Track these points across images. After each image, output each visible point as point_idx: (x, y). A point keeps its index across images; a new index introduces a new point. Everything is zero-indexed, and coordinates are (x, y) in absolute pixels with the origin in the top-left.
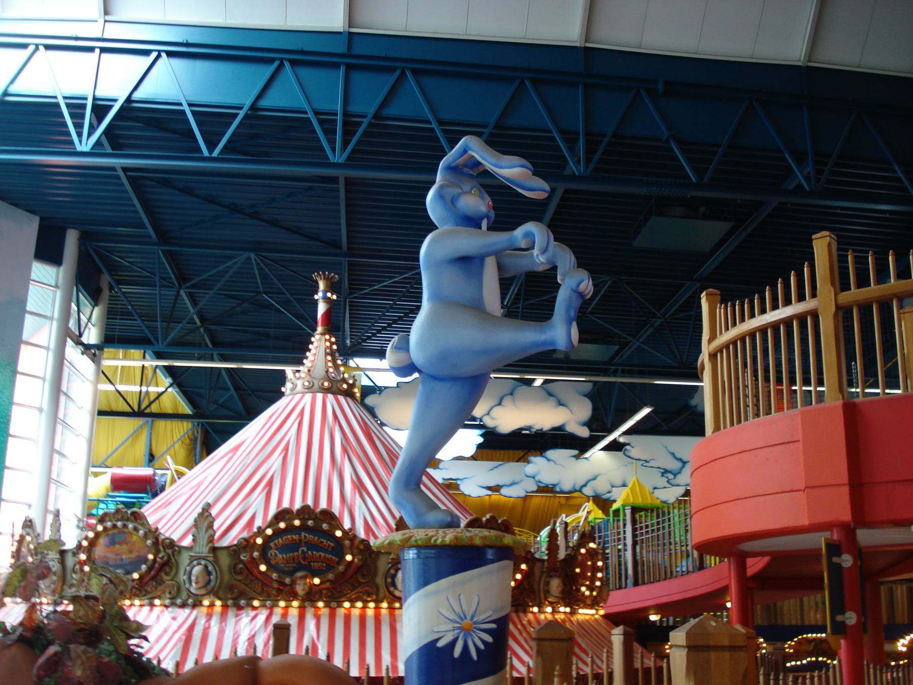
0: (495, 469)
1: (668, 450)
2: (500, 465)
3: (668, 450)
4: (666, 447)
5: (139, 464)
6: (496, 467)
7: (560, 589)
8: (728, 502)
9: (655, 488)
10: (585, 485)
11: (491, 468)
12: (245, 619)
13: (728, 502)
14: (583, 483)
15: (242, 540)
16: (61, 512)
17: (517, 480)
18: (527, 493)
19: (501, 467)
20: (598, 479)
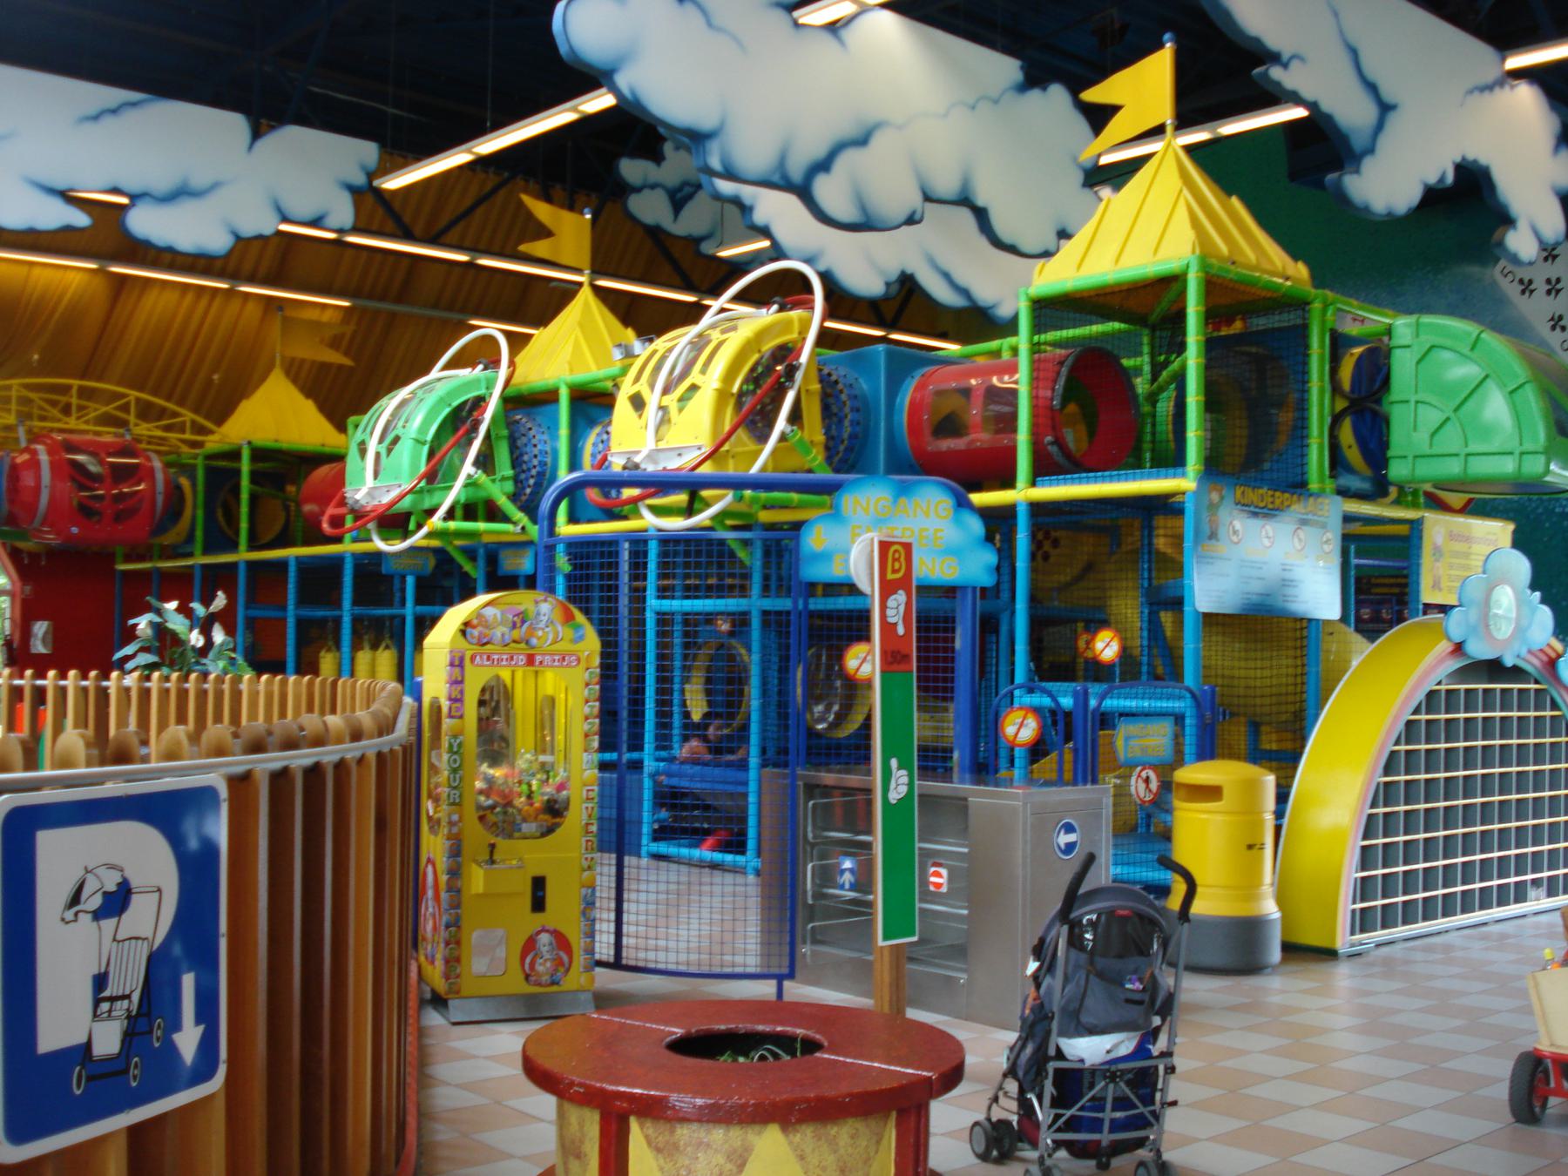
0: (109, 121)
1: (1341, 33)
2: (134, 104)
3: (1341, 33)
4: (1336, 14)
5: (299, 535)
6: (114, 111)
7: (1310, 385)
8: (1129, 235)
9: (964, 201)
10: (823, 165)
11: (93, 111)
12: (775, 729)
13: (1129, 235)
14: (819, 151)
15: (483, 738)
16: (400, 443)
17: (198, 180)
18: (286, 220)
19: (131, 116)
20: (877, 141)
